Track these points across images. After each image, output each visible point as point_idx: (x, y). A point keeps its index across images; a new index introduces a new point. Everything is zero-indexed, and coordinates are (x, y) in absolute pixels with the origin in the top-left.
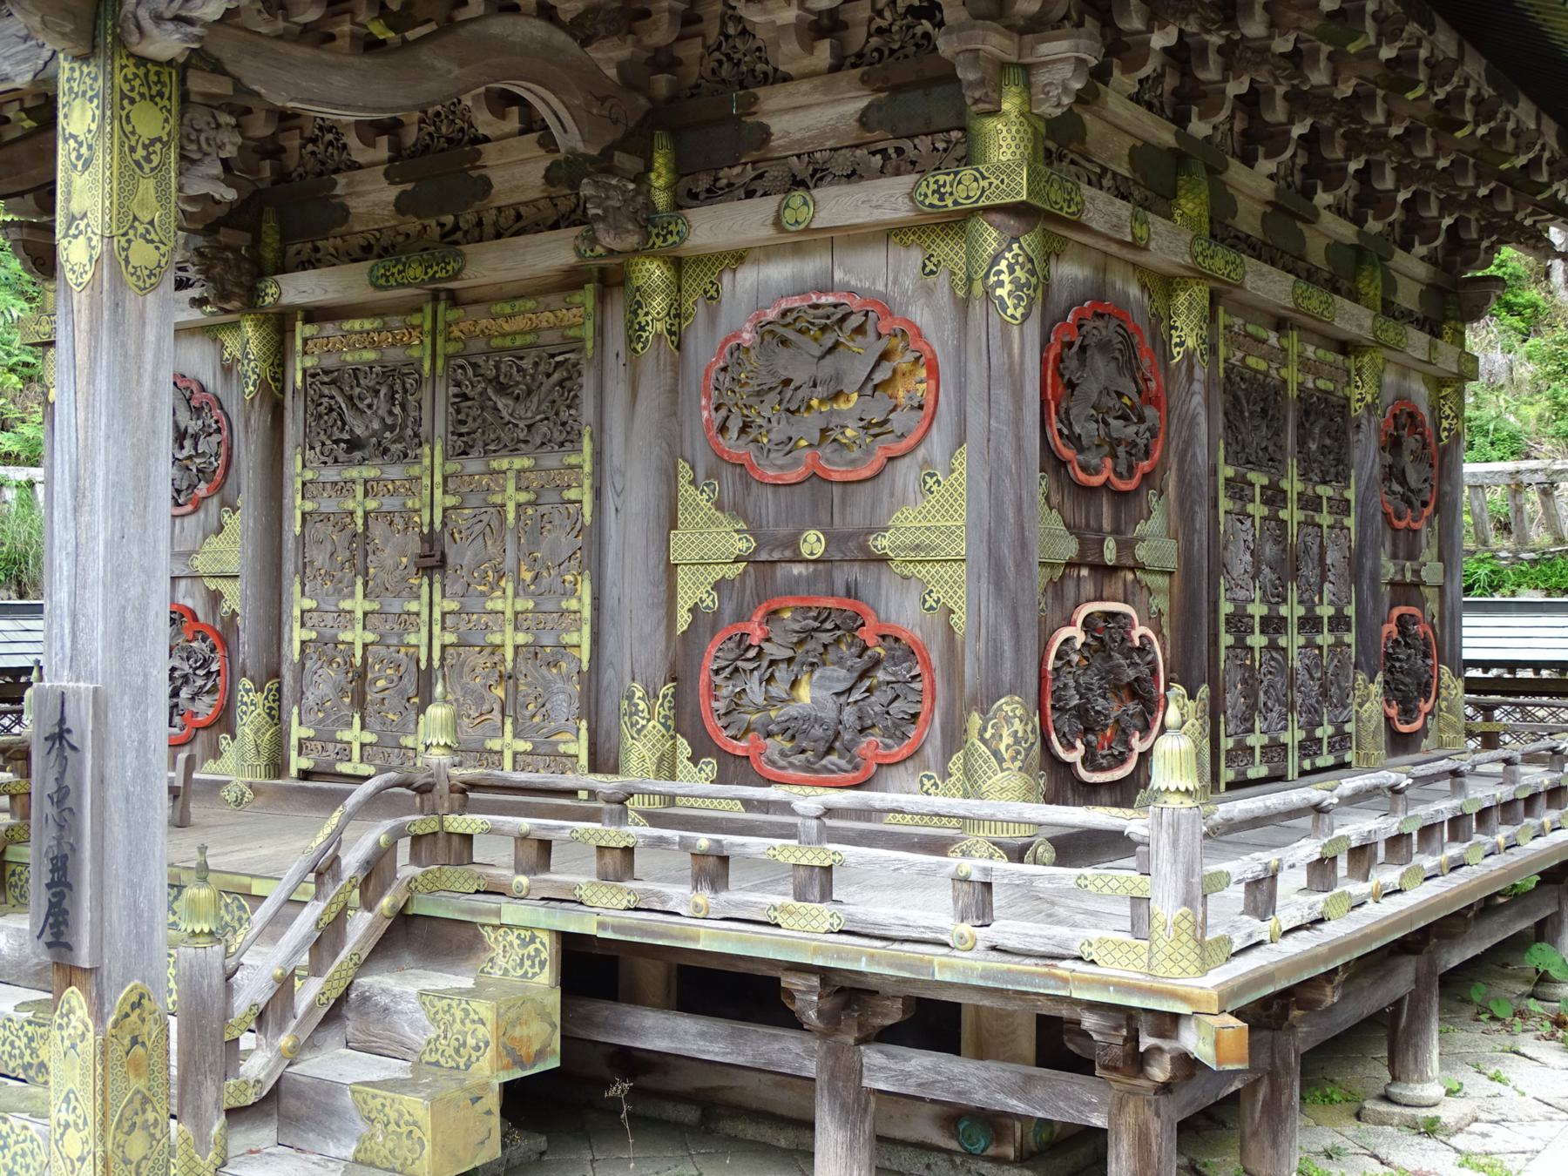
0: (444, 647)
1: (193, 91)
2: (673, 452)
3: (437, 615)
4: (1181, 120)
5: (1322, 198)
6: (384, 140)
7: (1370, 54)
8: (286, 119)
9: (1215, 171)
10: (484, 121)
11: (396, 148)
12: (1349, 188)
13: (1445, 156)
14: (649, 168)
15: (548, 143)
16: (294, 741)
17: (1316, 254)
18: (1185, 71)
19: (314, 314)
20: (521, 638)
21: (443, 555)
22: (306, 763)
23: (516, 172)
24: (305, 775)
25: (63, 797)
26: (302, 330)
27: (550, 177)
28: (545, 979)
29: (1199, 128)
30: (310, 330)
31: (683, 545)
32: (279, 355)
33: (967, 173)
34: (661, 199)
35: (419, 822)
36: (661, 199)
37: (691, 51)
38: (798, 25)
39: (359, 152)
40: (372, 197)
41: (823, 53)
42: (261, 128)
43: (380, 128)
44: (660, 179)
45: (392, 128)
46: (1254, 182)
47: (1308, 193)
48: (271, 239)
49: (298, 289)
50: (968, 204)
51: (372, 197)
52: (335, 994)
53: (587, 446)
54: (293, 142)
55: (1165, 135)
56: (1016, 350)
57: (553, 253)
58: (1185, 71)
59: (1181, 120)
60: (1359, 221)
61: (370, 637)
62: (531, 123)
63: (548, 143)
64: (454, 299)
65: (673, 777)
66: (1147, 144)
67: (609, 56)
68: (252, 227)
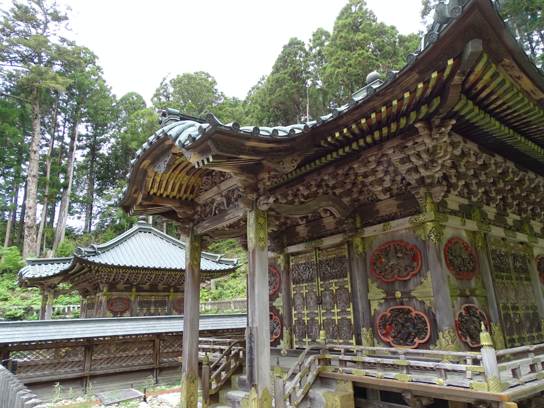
0: (321, 292)
1: (270, 215)
2: (366, 277)
3: (319, 285)
4: (469, 198)
5: (509, 211)
6: (305, 220)
7: (512, 180)
8: (287, 218)
9: (480, 208)
10: (323, 215)
11: (307, 222)
12: (515, 208)
13: (539, 198)
14: (355, 220)
15: (335, 218)
16: (293, 314)
17: (510, 222)
18: (469, 189)
19: (293, 254)
20: (339, 318)
21: (322, 300)
22: (297, 346)
23: (329, 222)
24: (297, 348)
25: (251, 348)
26: (292, 258)
27: (336, 224)
28: (351, 391)
29: (474, 199)
30: (293, 258)
31: (370, 296)
32: (287, 262)
33: (421, 216)
34: (358, 225)
35: (320, 356)
36: (358, 225)
37: (361, 198)
38: (382, 190)
39: (300, 222)
40: (302, 230)
41: (388, 196)
42: (283, 220)
43: (304, 217)
44: (358, 219)
45: (306, 217)
46: (491, 211)
47: (505, 210)
48: (285, 241)
49: (292, 249)
50: (422, 221)
51: (302, 230)
52: (306, 392)
53: (348, 275)
54: (289, 221)
55: (465, 202)
56: (442, 29)
57: (338, 239)
58: (469, 189)
59: (469, 198)
60: (520, 215)
61: (307, 291)
62: (332, 214)
63: (335, 218)
64: (320, 249)
65: (374, 346)
66: (462, 204)
67: (346, 200)
68: (282, 237)
